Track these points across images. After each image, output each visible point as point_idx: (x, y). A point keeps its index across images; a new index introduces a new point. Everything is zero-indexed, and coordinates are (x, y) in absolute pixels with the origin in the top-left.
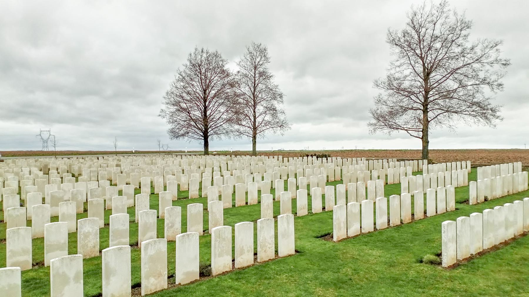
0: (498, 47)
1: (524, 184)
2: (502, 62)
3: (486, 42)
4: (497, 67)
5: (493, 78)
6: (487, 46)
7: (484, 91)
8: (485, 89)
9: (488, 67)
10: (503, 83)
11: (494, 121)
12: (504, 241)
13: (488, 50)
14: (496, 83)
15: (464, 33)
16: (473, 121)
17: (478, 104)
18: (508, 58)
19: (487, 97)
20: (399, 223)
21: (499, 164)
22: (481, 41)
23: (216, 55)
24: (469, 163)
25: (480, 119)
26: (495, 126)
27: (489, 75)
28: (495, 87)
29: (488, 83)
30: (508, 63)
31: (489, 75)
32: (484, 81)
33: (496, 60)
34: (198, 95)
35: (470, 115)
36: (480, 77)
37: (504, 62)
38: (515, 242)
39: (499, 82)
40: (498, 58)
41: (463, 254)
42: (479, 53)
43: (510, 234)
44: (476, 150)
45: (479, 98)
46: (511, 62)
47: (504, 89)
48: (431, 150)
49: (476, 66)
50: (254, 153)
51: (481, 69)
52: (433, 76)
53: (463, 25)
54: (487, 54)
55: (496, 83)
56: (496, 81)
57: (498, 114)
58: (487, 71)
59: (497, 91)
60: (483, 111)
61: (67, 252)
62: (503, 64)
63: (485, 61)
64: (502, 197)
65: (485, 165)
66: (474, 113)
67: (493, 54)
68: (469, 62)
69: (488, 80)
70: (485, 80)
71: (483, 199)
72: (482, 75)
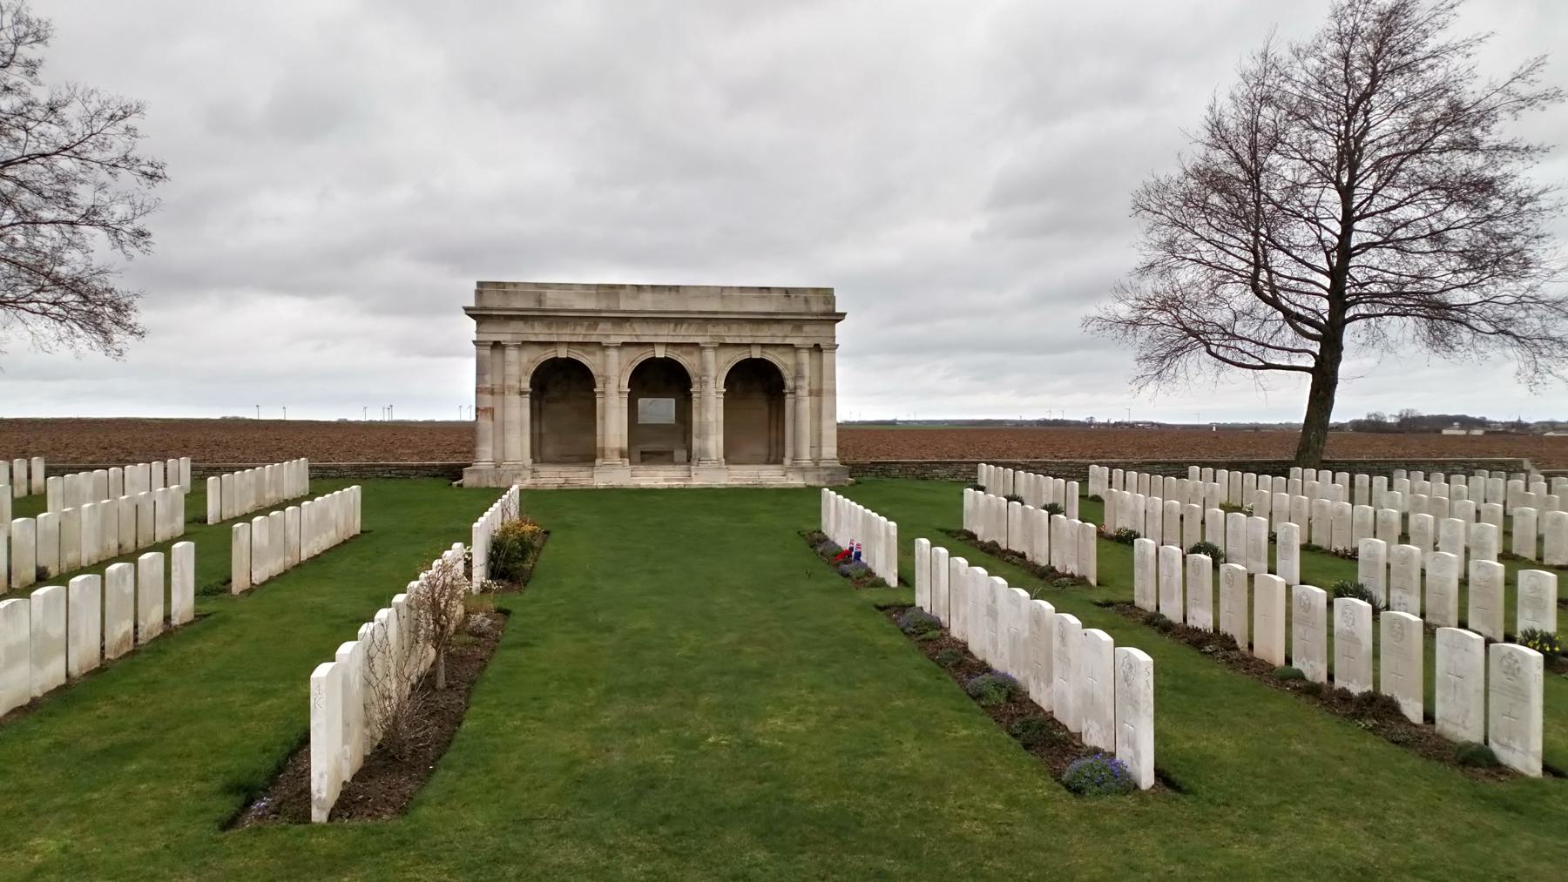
0: (130, 121)
1: (172, 520)
2: (143, 168)
3: (94, 98)
5: (121, 210)
6: (98, 113)
8: (96, 238)
9: (103, 176)
10: (147, 229)
11: (119, 336)
12: (27, 701)
13: (102, 124)
14: (128, 228)
15: (25, 52)
16: (52, 334)
17: (74, 285)
21: (121, 463)
22: (78, 93)
23: (1527, 263)
24: (185, 464)
25: (76, 327)
26: (121, 352)
27: (106, 198)
28: (124, 237)
29: (105, 225)
30: (160, 172)
31: (106, 198)
32: (91, 216)
33: (125, 159)
34: (33, 306)
35: (45, 313)
36: (80, 203)
37: (149, 170)
38: (67, 694)
39: (138, 223)
40: (131, 155)
41: (259, 576)
42: (78, 129)
43: (52, 674)
45: (73, 263)
48: (1340, 427)
49: (65, 164)
51: (81, 176)
53: (23, 28)
54: (100, 137)
55: (128, 228)
56: (128, 221)
57: (133, 318)
60: (96, 309)
61: (1361, 556)
62: (145, 173)
63: (96, 155)
64: (345, 542)
65: (76, 471)
66: (56, 309)
67: (119, 145)
68: (44, 148)
69: (105, 215)
70: (95, 213)
71: (31, 574)
72: (85, 196)
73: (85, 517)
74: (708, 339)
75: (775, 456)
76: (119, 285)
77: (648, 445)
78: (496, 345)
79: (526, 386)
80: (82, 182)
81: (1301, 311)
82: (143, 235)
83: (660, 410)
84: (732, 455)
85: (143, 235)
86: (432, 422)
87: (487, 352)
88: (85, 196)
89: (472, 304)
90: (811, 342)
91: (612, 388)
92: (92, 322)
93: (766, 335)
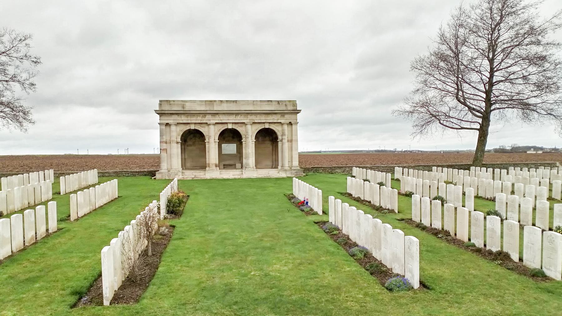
0: (27, 41)
1: (48, 193)
2: (32, 59)
3: (13, 33)
4: (27, 63)
5: (24, 76)
7: (13, 89)
8: (16, 86)
9: (17, 62)
11: (25, 124)
14: (27, 82)
17: (8, 105)
18: (38, 56)
19: (16, 96)
20: (10, 254)
24: (51, 172)
25: (10, 121)
28: (26, 86)
29: (19, 81)
30: (38, 61)
31: (19, 71)
32: (14, 78)
33: (26, 56)
36: (9, 73)
37: (35, 60)
39: (31, 80)
44: (23, 156)
46: (41, 60)
47: (37, 90)
50: (479, 158)
51: (10, 63)
52: (479, 68)
55: (27, 82)
56: (27, 80)
58: (17, 67)
59: (30, 91)
63: (15, 55)
64: (112, 201)
65: (12, 175)
69: (19, 78)
70: (15, 77)
72: (11, 70)
73: (15, 192)
74: (248, 121)
75: (275, 166)
76: (25, 104)
77: (226, 162)
78: (167, 124)
79: (179, 140)
80: (10, 65)
81: (474, 107)
82: (33, 85)
83: (230, 148)
84: (258, 165)
85: (33, 85)
86: (144, 155)
87: (164, 127)
88: (11, 70)
89: (158, 109)
90: (288, 121)
91: (212, 140)
92: (15, 118)
93: (271, 119)
